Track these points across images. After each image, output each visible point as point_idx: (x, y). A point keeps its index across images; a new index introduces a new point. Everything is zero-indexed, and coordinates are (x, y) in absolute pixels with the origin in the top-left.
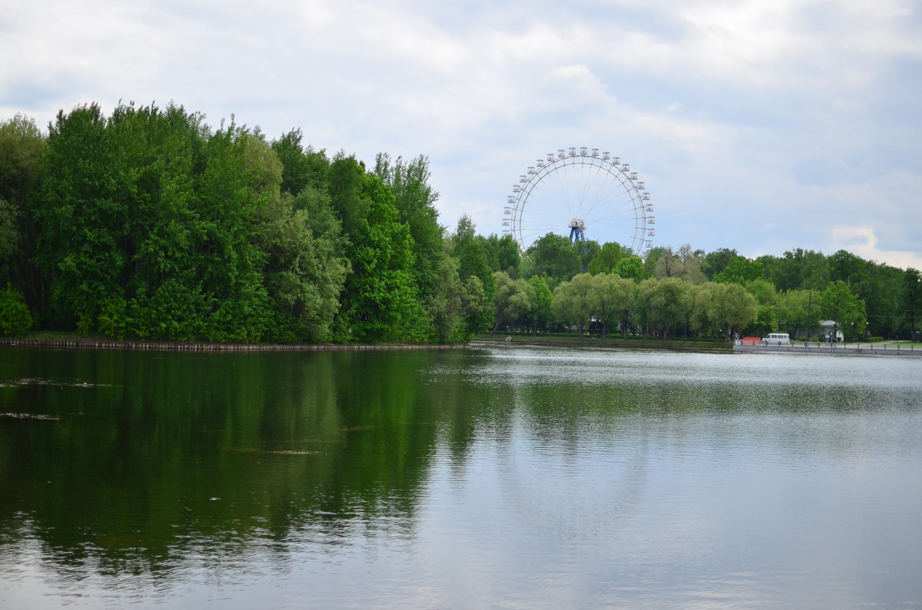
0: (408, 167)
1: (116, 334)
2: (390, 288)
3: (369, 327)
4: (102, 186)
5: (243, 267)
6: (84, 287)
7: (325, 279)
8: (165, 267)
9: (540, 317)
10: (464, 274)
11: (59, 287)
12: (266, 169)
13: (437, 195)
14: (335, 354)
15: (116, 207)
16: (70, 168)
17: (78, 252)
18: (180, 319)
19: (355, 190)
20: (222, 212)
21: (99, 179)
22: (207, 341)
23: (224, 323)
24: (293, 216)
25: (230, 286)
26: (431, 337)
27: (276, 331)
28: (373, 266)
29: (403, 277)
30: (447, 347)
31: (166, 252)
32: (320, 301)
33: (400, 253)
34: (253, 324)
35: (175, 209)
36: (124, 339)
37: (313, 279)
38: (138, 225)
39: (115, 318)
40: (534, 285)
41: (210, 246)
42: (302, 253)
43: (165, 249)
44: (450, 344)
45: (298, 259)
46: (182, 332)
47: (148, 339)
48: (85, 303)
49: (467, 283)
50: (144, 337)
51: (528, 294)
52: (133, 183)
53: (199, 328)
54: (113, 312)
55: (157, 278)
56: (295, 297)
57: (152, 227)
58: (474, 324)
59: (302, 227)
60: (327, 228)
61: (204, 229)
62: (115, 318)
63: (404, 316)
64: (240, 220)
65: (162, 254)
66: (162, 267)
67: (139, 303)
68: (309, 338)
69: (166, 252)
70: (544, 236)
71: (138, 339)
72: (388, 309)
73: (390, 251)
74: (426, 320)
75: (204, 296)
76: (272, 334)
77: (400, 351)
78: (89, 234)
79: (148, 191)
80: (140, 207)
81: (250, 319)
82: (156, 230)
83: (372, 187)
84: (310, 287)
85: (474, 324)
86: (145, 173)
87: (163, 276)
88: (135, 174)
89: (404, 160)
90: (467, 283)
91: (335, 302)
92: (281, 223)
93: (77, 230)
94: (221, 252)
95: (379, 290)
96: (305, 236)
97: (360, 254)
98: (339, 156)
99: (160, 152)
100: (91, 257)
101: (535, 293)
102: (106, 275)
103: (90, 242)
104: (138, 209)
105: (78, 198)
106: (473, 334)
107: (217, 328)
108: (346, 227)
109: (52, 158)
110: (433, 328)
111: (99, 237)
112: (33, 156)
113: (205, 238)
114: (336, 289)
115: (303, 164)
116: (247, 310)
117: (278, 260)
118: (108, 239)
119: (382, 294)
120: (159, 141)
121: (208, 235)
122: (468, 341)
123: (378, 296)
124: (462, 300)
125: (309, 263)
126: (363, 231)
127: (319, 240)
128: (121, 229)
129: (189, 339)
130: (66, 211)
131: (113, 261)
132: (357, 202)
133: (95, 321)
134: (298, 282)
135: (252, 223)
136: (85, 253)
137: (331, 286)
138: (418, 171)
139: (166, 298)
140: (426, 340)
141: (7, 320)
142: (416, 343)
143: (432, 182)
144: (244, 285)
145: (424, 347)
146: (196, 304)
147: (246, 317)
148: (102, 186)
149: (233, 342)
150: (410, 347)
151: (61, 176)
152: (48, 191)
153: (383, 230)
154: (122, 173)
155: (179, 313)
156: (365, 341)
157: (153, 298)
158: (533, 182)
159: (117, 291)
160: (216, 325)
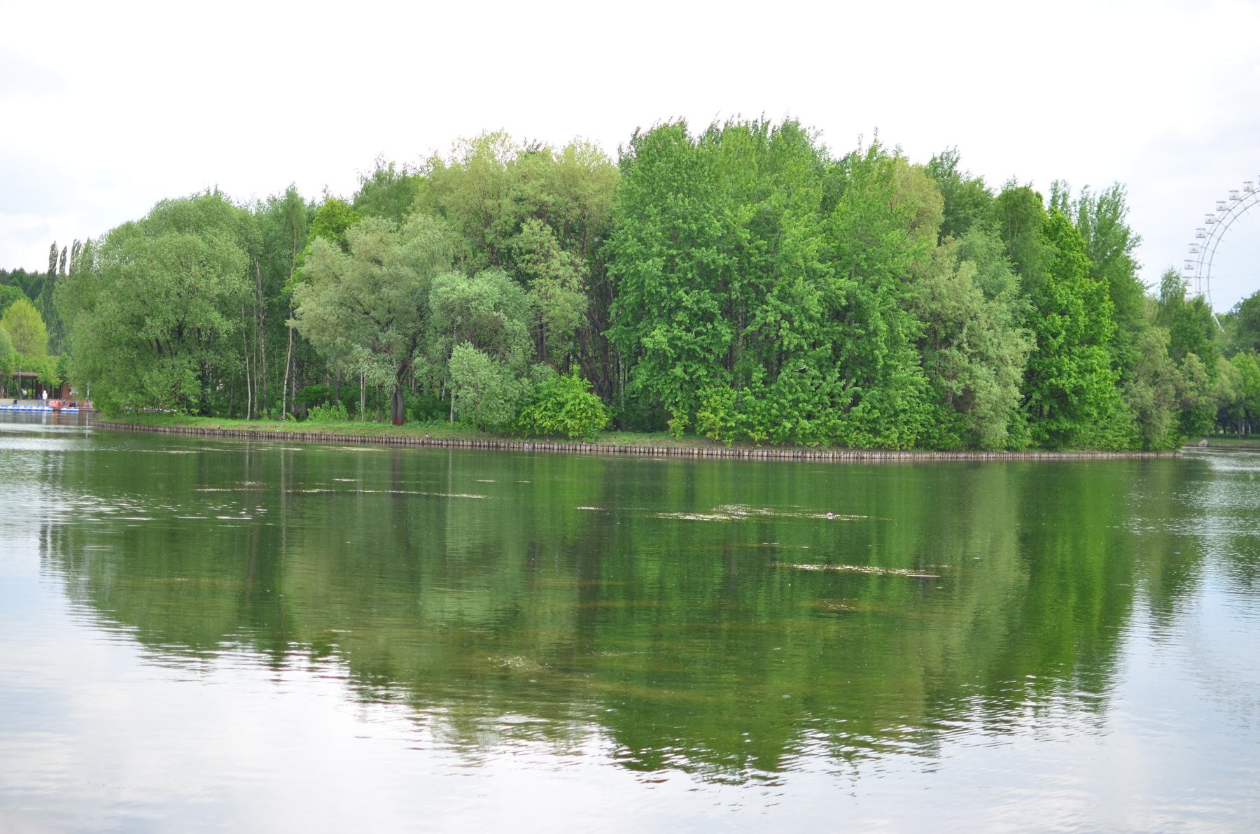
0: (1097, 201)
1: (722, 437)
2: (1082, 371)
3: (1054, 427)
4: (701, 231)
5: (893, 342)
6: (678, 371)
7: (1001, 359)
8: (790, 343)
9: (1247, 412)
10: (1177, 351)
11: (643, 371)
12: (922, 205)
13: (1138, 239)
14: (1011, 465)
15: (722, 259)
16: (655, 207)
17: (670, 322)
18: (810, 416)
19: (1035, 232)
20: (864, 265)
21: (696, 220)
22: (843, 446)
23: (868, 422)
24: (956, 270)
25: (875, 370)
26: (1132, 442)
27: (935, 432)
28: (1061, 339)
29: (1101, 355)
30: (1152, 455)
31: (791, 323)
32: (996, 389)
33: (1096, 321)
34: (905, 423)
35: (801, 262)
36: (732, 444)
37: (985, 358)
38: (751, 284)
39: (722, 414)
40: (1239, 366)
41: (844, 313)
42: (969, 323)
43: (787, 317)
44: (1156, 450)
45: (965, 331)
46: (812, 434)
47: (765, 444)
48: (679, 393)
49: (1182, 363)
50: (761, 441)
51: (1231, 378)
52: (745, 226)
53: (834, 428)
54: (718, 404)
55: (776, 360)
56: (962, 385)
57: (770, 286)
58: (1188, 423)
59: (969, 285)
60: (1001, 287)
61: (840, 289)
62: (722, 414)
63: (1103, 411)
64: (889, 276)
65: (786, 325)
66: (786, 343)
67: (754, 394)
68: (975, 442)
69: (791, 323)
70: (1249, 297)
71: (751, 443)
72: (1083, 402)
73: (1082, 320)
74: (1127, 417)
75: (843, 382)
76: (929, 437)
77: (1092, 461)
78: (685, 297)
79: (762, 238)
80: (753, 259)
81: (902, 416)
82: (775, 292)
83: (1055, 230)
84: (982, 370)
85: (1188, 423)
86: (758, 212)
87: (784, 356)
88: (747, 213)
89: (1091, 190)
90: (1182, 363)
91: (1016, 392)
92: (942, 279)
93: (669, 292)
94: (863, 322)
95: (1070, 375)
96: (974, 299)
97: (1043, 324)
98: (1009, 184)
99: (776, 183)
100: (688, 330)
101: (1240, 378)
102: (707, 355)
103: (686, 308)
104: (749, 262)
105: (670, 247)
106: (1185, 437)
107: (858, 428)
108: (1025, 287)
109: (630, 194)
110: (1136, 428)
111: (698, 302)
112: (601, 190)
113: (844, 302)
114: (1017, 374)
115: (962, 196)
116: (900, 403)
117: (938, 334)
118: (711, 305)
119: (1072, 380)
120: (774, 167)
121: (847, 298)
122: (1178, 446)
123: (1067, 384)
124: (1177, 389)
125: (980, 338)
126: (1047, 291)
127: (991, 303)
128: (727, 290)
129: (821, 444)
130: (654, 266)
131: (717, 335)
132: (1035, 251)
133: (693, 419)
134: (966, 363)
135: (902, 280)
136: (680, 323)
137: (1011, 369)
138: (1111, 206)
139: (791, 386)
140: (1126, 445)
141: (573, 417)
142: (1113, 450)
143: (1131, 220)
144: (895, 368)
145: (1123, 455)
146: (831, 395)
147: (896, 414)
148: (701, 231)
149: (880, 448)
150: (1105, 455)
151: (644, 217)
152: (626, 240)
153: (1072, 289)
154: (727, 212)
155: (809, 407)
156: (1047, 447)
157: (773, 387)
158: (1225, 222)
159: (722, 377)
160: (858, 424)
